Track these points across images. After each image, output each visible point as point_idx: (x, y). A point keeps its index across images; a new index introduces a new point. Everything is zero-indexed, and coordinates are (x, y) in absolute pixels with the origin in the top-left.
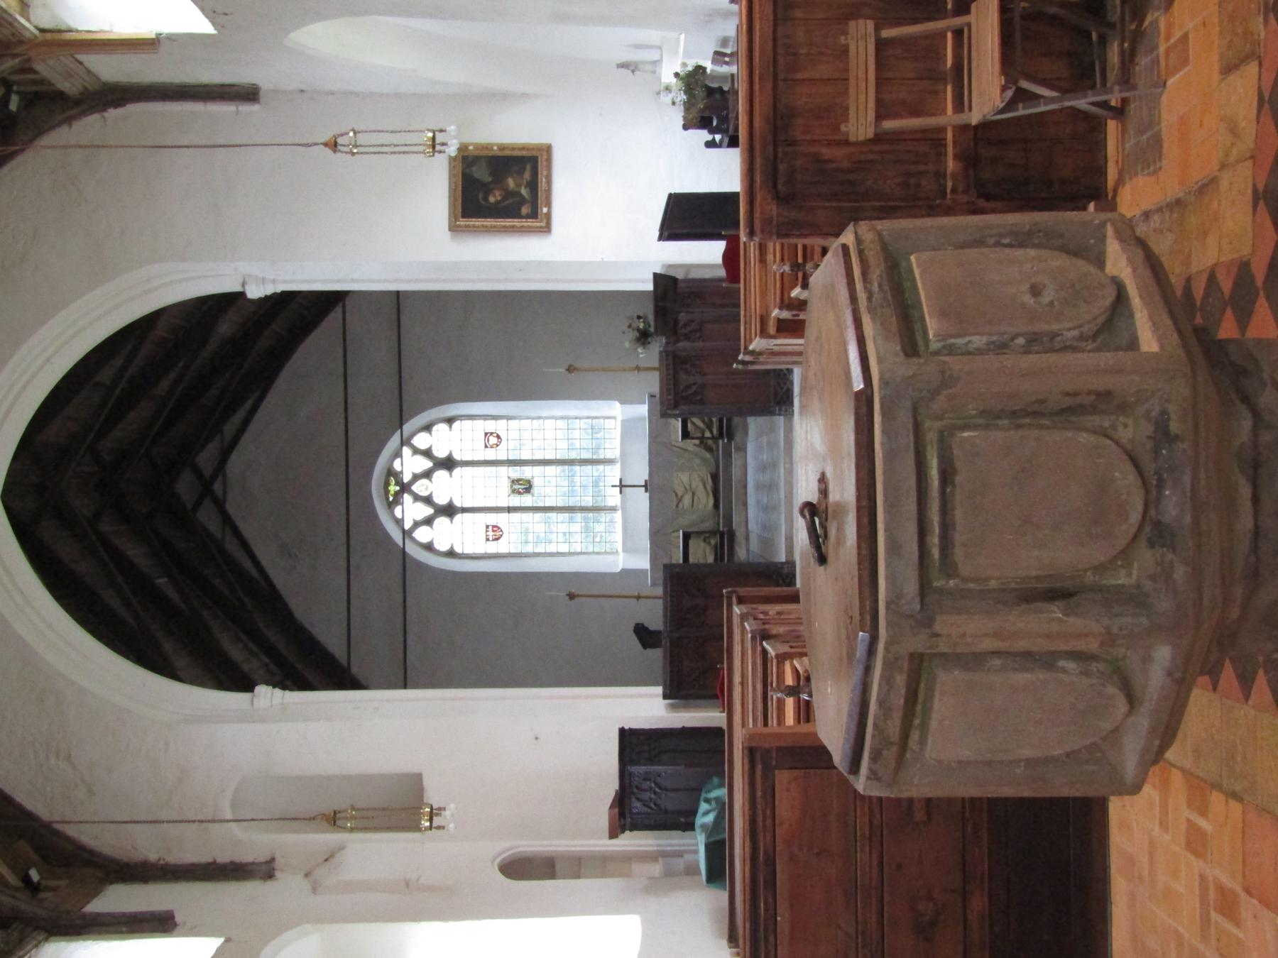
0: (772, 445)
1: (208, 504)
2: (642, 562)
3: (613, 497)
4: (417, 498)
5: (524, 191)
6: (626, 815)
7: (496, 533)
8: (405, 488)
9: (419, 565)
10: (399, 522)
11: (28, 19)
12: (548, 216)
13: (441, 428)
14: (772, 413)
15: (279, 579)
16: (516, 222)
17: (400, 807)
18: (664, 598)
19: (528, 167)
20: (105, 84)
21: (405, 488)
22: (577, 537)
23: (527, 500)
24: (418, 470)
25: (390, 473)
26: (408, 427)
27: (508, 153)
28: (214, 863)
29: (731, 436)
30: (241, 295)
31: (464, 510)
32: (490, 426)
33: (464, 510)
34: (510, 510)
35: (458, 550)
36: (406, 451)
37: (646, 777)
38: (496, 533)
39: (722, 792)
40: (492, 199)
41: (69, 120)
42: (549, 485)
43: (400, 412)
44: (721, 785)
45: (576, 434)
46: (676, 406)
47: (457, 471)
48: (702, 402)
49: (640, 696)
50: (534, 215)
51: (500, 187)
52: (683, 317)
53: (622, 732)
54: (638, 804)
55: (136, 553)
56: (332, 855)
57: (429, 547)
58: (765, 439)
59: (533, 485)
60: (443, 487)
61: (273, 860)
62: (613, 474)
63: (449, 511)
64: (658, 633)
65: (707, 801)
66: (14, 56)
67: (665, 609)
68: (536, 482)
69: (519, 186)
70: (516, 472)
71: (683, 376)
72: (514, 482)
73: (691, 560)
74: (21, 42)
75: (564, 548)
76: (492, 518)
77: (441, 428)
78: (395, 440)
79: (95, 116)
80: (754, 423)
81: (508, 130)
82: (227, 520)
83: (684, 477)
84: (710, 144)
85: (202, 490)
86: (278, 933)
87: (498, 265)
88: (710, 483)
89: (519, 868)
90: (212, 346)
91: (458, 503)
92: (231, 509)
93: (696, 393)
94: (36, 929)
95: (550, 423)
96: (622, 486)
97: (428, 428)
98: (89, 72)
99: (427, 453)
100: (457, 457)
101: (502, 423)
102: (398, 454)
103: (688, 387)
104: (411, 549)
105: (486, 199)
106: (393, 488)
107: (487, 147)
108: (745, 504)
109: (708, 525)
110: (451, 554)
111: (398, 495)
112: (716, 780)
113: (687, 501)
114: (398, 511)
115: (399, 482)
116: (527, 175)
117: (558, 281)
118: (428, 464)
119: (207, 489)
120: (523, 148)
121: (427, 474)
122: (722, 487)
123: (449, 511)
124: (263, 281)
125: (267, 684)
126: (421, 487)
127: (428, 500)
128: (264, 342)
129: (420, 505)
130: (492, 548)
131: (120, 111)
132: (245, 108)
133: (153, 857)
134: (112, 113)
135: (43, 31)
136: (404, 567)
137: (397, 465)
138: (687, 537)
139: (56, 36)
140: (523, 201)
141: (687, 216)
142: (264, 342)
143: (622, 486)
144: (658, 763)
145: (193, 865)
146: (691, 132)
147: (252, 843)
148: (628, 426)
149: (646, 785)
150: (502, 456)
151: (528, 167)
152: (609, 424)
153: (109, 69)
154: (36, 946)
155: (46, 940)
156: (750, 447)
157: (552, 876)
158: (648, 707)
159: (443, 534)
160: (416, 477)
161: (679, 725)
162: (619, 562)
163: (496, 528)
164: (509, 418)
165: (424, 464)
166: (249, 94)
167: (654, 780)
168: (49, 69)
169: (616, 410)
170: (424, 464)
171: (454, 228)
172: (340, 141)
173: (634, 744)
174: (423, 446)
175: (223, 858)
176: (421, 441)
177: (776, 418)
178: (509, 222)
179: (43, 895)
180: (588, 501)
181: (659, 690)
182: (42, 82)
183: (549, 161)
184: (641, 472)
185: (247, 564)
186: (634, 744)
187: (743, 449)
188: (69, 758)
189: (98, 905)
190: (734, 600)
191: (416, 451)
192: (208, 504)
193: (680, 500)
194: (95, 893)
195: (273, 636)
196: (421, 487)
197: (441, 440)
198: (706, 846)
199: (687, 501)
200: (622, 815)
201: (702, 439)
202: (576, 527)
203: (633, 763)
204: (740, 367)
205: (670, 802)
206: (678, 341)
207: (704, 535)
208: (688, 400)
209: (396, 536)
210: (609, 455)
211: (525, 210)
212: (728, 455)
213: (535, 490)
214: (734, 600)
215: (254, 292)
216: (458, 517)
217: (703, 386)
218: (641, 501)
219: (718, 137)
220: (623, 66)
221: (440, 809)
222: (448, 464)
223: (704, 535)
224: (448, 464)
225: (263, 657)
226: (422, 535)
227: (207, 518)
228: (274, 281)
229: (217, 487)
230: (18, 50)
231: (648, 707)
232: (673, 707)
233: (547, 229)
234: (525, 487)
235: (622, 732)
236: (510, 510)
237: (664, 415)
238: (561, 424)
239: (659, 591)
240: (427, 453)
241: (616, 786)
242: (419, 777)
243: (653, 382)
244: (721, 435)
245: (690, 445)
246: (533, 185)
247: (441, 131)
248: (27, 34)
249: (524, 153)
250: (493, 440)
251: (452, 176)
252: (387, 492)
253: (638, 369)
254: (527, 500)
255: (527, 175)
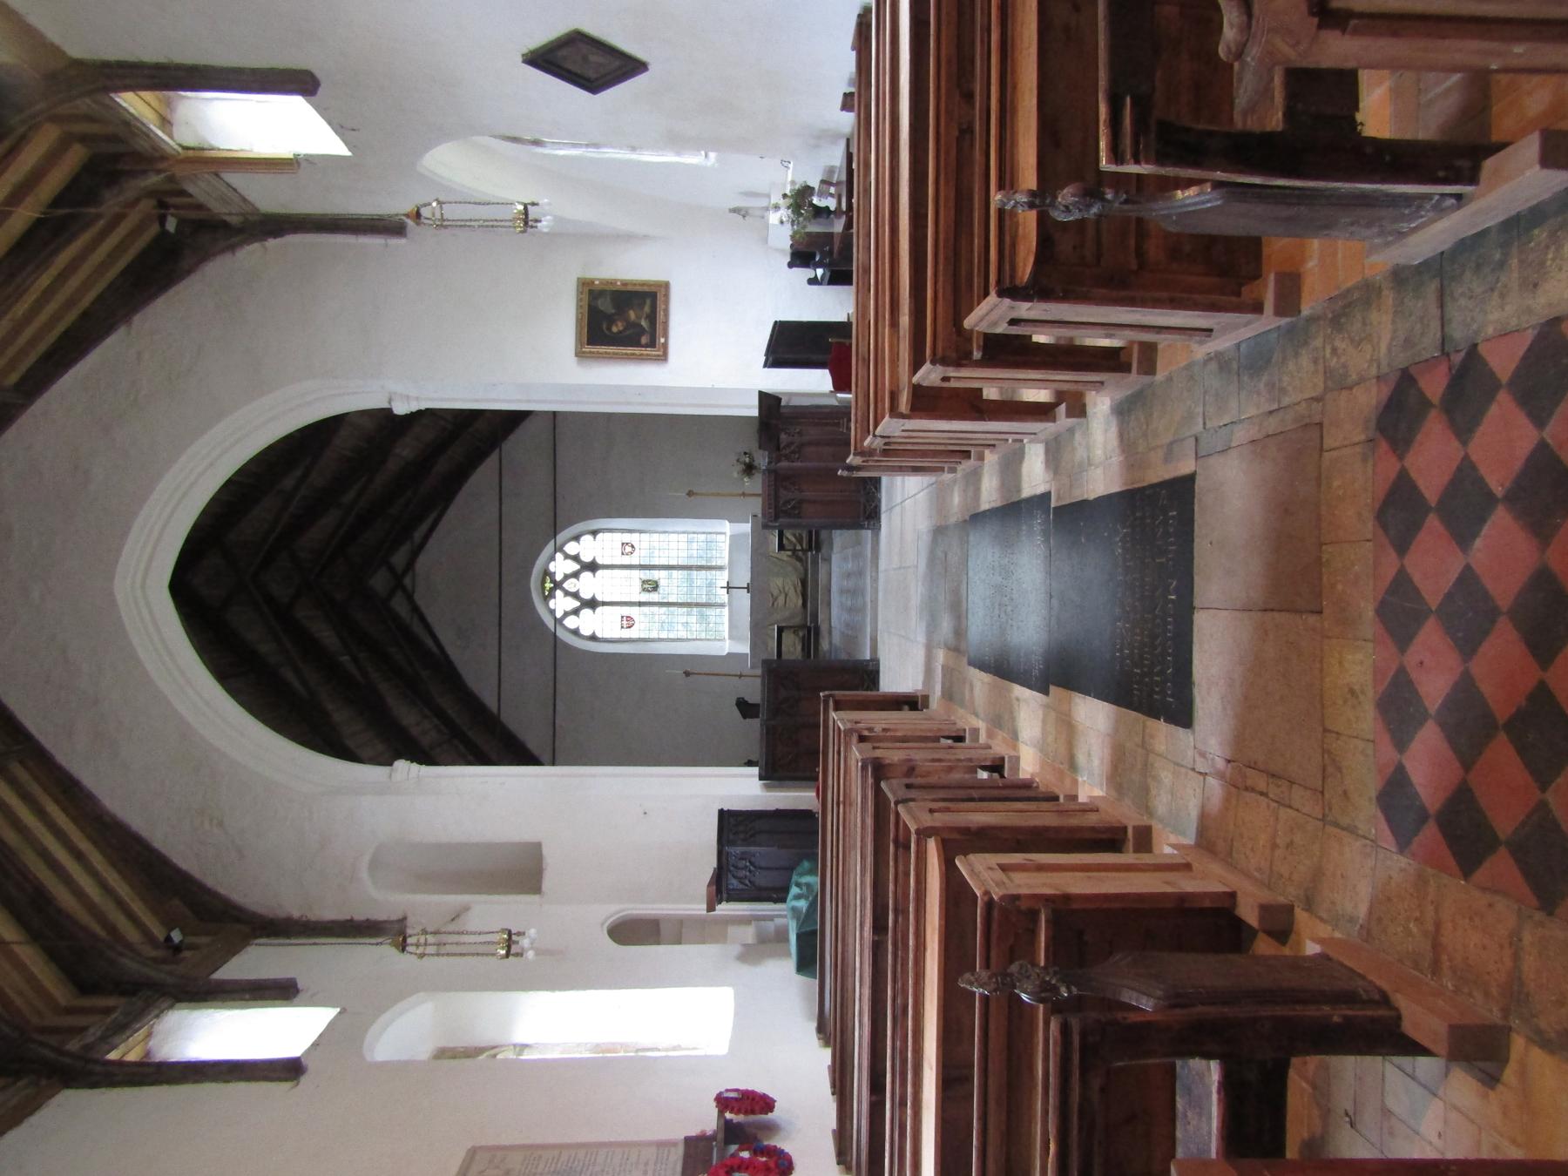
0: (858, 556)
1: (399, 594)
2: (744, 648)
3: (723, 596)
4: (567, 593)
5: (643, 323)
6: (722, 887)
7: (629, 622)
8: (557, 585)
9: (567, 646)
10: (552, 612)
11: (171, 137)
12: (665, 346)
13: (587, 539)
14: (862, 527)
15: (453, 653)
16: (637, 351)
17: (521, 871)
18: (763, 677)
19: (648, 302)
20: (256, 211)
21: (557, 585)
22: (695, 627)
23: (654, 597)
24: (569, 572)
25: (547, 573)
26: (560, 537)
27: (629, 288)
28: (351, 920)
29: (818, 549)
30: (389, 411)
31: (604, 604)
32: (627, 537)
33: (604, 604)
34: (640, 604)
35: (599, 635)
36: (559, 556)
37: (743, 857)
38: (629, 622)
39: (814, 880)
40: (615, 329)
41: (232, 248)
42: (672, 586)
43: (555, 523)
44: (812, 872)
45: (695, 546)
46: (776, 518)
47: (600, 573)
48: (799, 516)
49: (735, 776)
50: (652, 344)
51: (623, 319)
52: (783, 436)
53: (721, 812)
54: (734, 882)
55: (327, 636)
56: (458, 916)
57: (576, 632)
58: (850, 551)
59: (655, 586)
60: (588, 585)
61: (405, 919)
62: (722, 578)
63: (592, 604)
64: (756, 706)
65: (798, 885)
66: (159, 172)
67: (763, 684)
68: (662, 583)
69: (639, 317)
70: (647, 575)
71: (783, 492)
72: (644, 582)
73: (785, 657)
74: (164, 157)
75: (682, 634)
76: (626, 611)
77: (587, 539)
78: (550, 547)
79: (256, 246)
80: (840, 538)
81: (629, 267)
82: (415, 609)
83: (779, 582)
84: (813, 281)
85: (367, 586)
86: (381, 1010)
87: (620, 389)
88: (799, 588)
89: (630, 931)
90: (393, 465)
91: (599, 598)
92: (419, 599)
93: (794, 508)
94: (164, 995)
95: (673, 537)
96: (729, 588)
97: (577, 538)
98: (244, 200)
99: (576, 558)
100: (600, 561)
101: (636, 535)
102: (552, 558)
103: (788, 502)
104: (561, 633)
105: (609, 329)
106: (548, 585)
107: (612, 282)
108: (829, 604)
109: (797, 621)
110: (593, 638)
111: (552, 590)
112: (806, 865)
113: (781, 600)
114: (552, 604)
115: (553, 581)
116: (647, 309)
117: (673, 405)
118: (576, 567)
119: (398, 582)
120: (643, 284)
121: (576, 575)
122: (809, 590)
123: (592, 604)
124: (408, 397)
125: (842, 527)
126: (570, 585)
127: (576, 595)
128: (442, 466)
129: (569, 599)
130: (626, 634)
131: (278, 240)
132: (395, 242)
133: (296, 914)
134: (272, 243)
135: (187, 148)
136: (554, 649)
137: (552, 567)
138: (780, 630)
139: (198, 154)
140: (643, 331)
141: (792, 344)
142: (442, 466)
143: (729, 588)
144: (755, 844)
145: (333, 922)
146: (795, 269)
147: (383, 901)
148: (734, 539)
149: (742, 864)
150: (634, 560)
151: (648, 302)
152: (720, 538)
153: (267, 197)
154: (157, 1016)
155: (171, 1007)
156: (835, 558)
157: (657, 940)
158: (744, 787)
159: (587, 622)
160: (567, 577)
161: (771, 807)
162: (726, 647)
163: (629, 618)
164: (641, 532)
165: (573, 567)
166: (390, 227)
167: (754, 857)
168: (200, 189)
169: (726, 527)
170: (573, 567)
171: (579, 354)
172: (425, 212)
173: (733, 824)
174: (573, 553)
175: (360, 915)
176: (571, 548)
177: (864, 532)
178: (630, 350)
179: (187, 954)
180: (704, 600)
181: (755, 770)
182: (200, 207)
183: (667, 296)
184: (744, 578)
185: (429, 642)
186: (733, 824)
187: (828, 560)
188: (221, 824)
189: (230, 971)
190: (831, 704)
191: (567, 556)
192: (399, 594)
193: (776, 599)
194: (233, 950)
195: (447, 703)
196: (570, 585)
197: (587, 548)
198: (799, 936)
199: (781, 600)
200: (719, 891)
201: (794, 551)
202: (693, 619)
203: (732, 843)
204: (845, 473)
205: (762, 879)
206: (779, 460)
207: (795, 629)
208: (788, 514)
209: (550, 623)
210: (719, 563)
211: (644, 340)
212: (815, 563)
213: (661, 590)
214: (831, 704)
215: (401, 409)
216: (599, 609)
217: (801, 502)
218: (745, 599)
219: (820, 272)
220: (735, 211)
221: (519, 934)
222: (593, 567)
223: (795, 629)
224: (593, 567)
225: (435, 720)
226: (571, 622)
227: (399, 605)
228: (417, 399)
229: (407, 581)
230: (161, 166)
231: (744, 787)
232: (767, 787)
233: (663, 357)
234: (654, 586)
235: (721, 812)
236: (640, 604)
237: (765, 526)
238: (683, 537)
239: (759, 672)
240: (576, 558)
241: (715, 865)
242: (538, 846)
243: (756, 505)
244: (810, 549)
245: (785, 555)
246: (652, 318)
247: (533, 204)
248: (169, 151)
249: (646, 289)
250: (628, 549)
251: (579, 307)
252: (543, 588)
253: (744, 494)
254: (654, 597)
255: (647, 309)
